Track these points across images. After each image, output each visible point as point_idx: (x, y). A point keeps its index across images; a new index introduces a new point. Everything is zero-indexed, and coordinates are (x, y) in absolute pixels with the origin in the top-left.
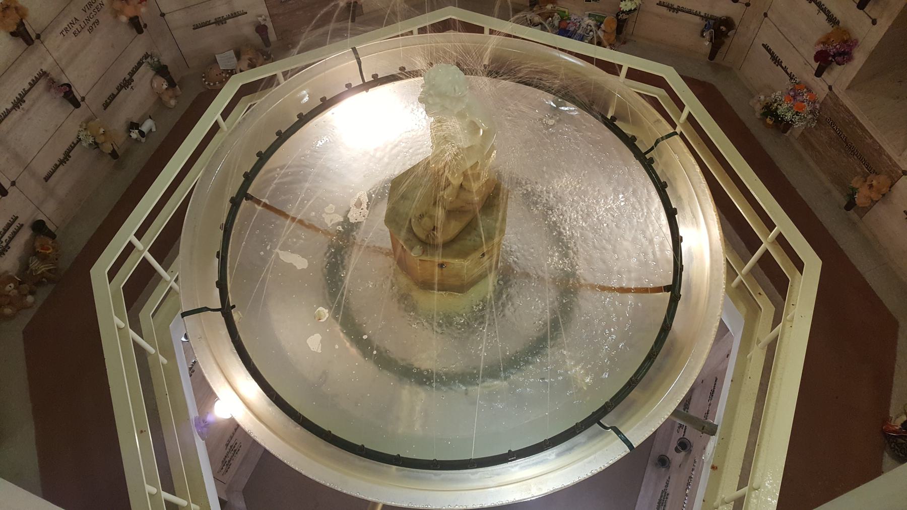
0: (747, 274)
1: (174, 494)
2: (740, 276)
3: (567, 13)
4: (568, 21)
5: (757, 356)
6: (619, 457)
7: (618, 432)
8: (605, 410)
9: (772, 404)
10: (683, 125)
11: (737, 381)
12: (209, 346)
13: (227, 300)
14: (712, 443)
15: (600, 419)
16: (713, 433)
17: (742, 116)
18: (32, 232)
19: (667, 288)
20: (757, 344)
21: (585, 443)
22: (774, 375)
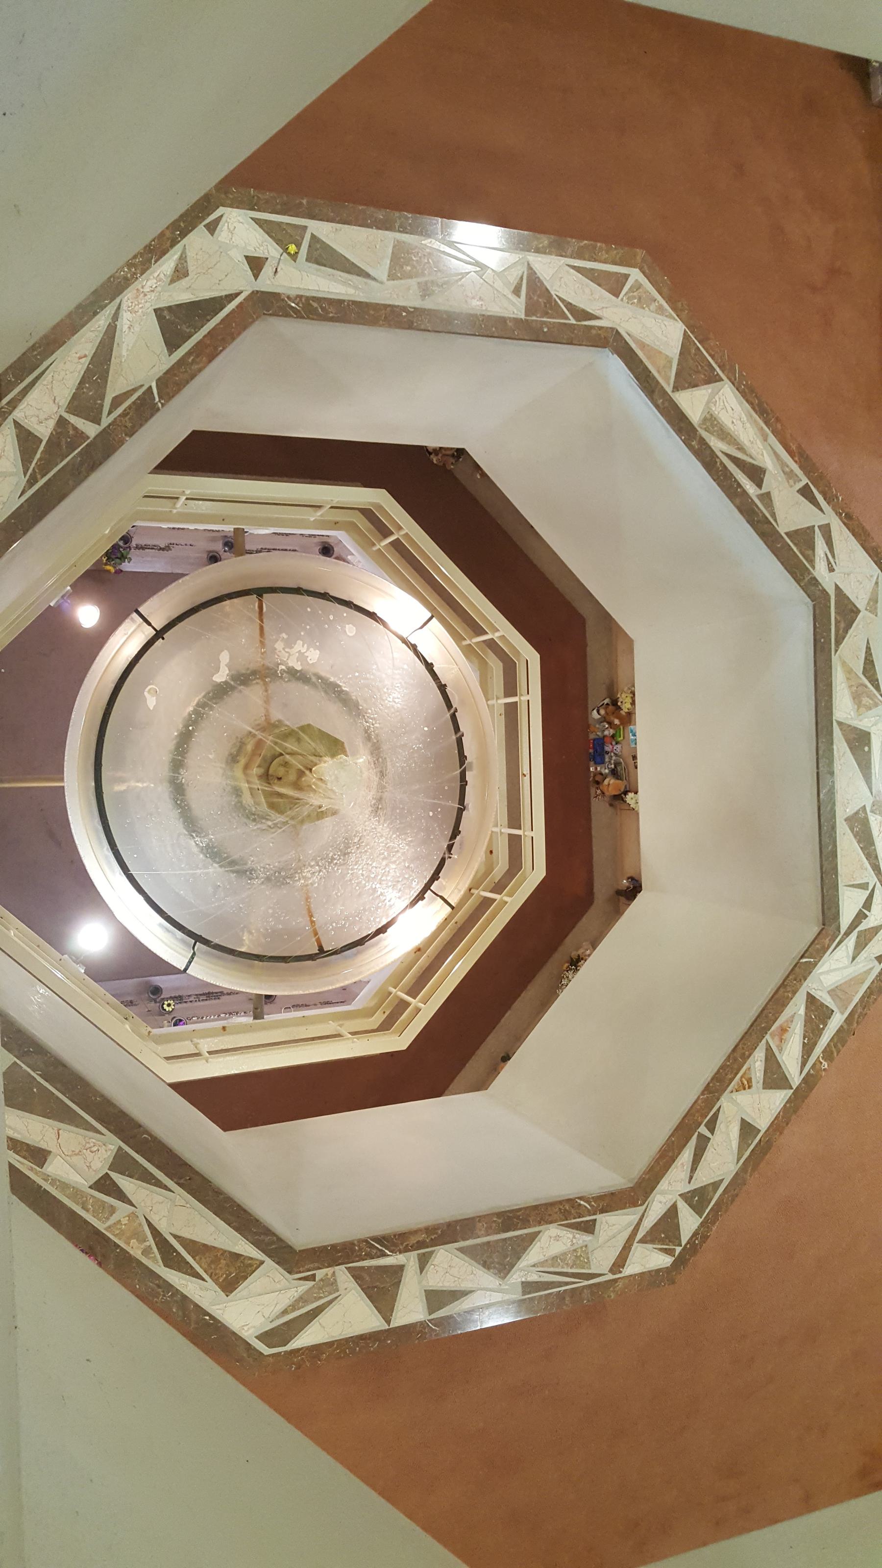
0: (398, 997)
1: (484, 641)
2: (394, 990)
3: (620, 739)
4: (614, 743)
5: (330, 1028)
6: (175, 964)
7: (192, 958)
8: (206, 942)
9: (306, 1047)
10: (501, 899)
11: (305, 1021)
12: (386, 593)
13: (388, 578)
14: (248, 1020)
15: (200, 942)
16: (255, 1018)
17: (569, 940)
18: (607, 349)
19: (321, 949)
20: (339, 1025)
21: (177, 938)
22: (188, 1061)
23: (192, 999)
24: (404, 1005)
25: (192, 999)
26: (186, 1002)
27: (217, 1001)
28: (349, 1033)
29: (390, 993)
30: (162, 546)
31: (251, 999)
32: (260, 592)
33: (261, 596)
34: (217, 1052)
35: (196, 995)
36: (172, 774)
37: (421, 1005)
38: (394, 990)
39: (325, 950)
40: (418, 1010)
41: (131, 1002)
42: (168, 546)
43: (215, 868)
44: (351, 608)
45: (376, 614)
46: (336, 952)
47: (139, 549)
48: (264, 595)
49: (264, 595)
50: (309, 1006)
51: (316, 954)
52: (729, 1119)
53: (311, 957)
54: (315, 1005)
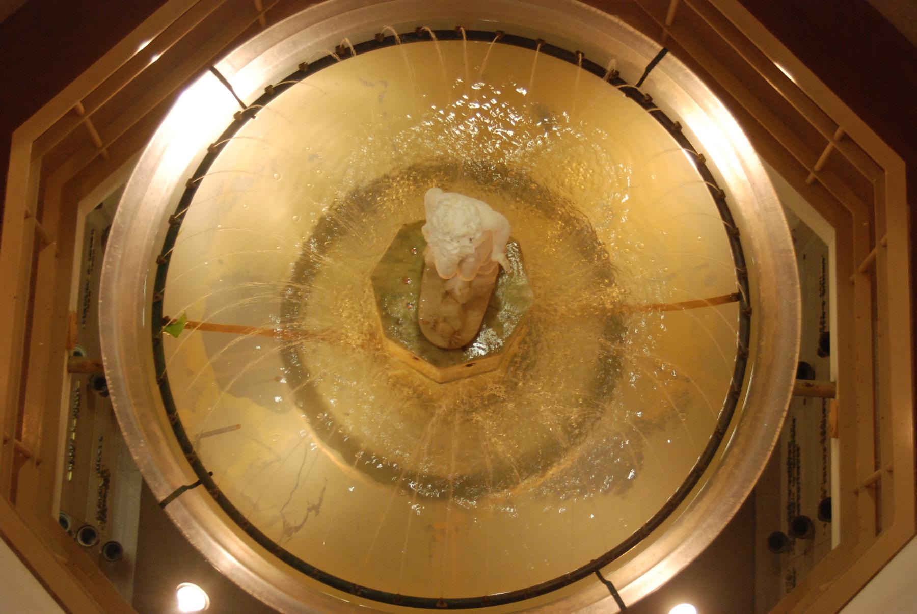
2: (812, 176)
19: (737, 297)
23: (794, 490)
24: (835, 165)
25: (794, 490)
26: (799, 498)
27: (802, 452)
28: (871, 251)
29: (815, 182)
30: (102, 482)
31: (805, 402)
32: (159, 321)
33: (166, 320)
34: (877, 456)
35: (789, 482)
36: (295, 391)
37: (838, 133)
38: (812, 176)
39: (737, 292)
40: (845, 138)
41: (789, 578)
42: (103, 473)
43: (515, 279)
44: (198, 183)
45: (212, 145)
46: (743, 277)
47: (105, 515)
48: (164, 315)
49: (164, 315)
50: (824, 314)
51: (742, 307)
52: (792, 484)
53: (746, 315)
54: (824, 303)
